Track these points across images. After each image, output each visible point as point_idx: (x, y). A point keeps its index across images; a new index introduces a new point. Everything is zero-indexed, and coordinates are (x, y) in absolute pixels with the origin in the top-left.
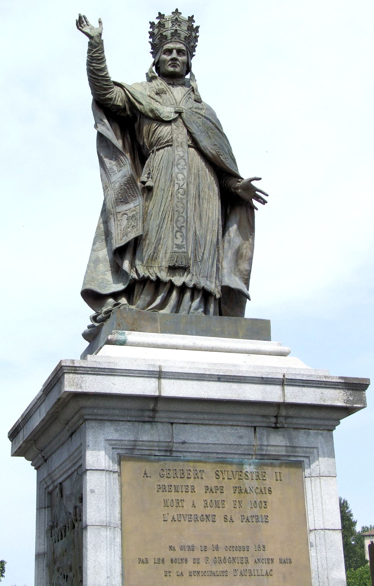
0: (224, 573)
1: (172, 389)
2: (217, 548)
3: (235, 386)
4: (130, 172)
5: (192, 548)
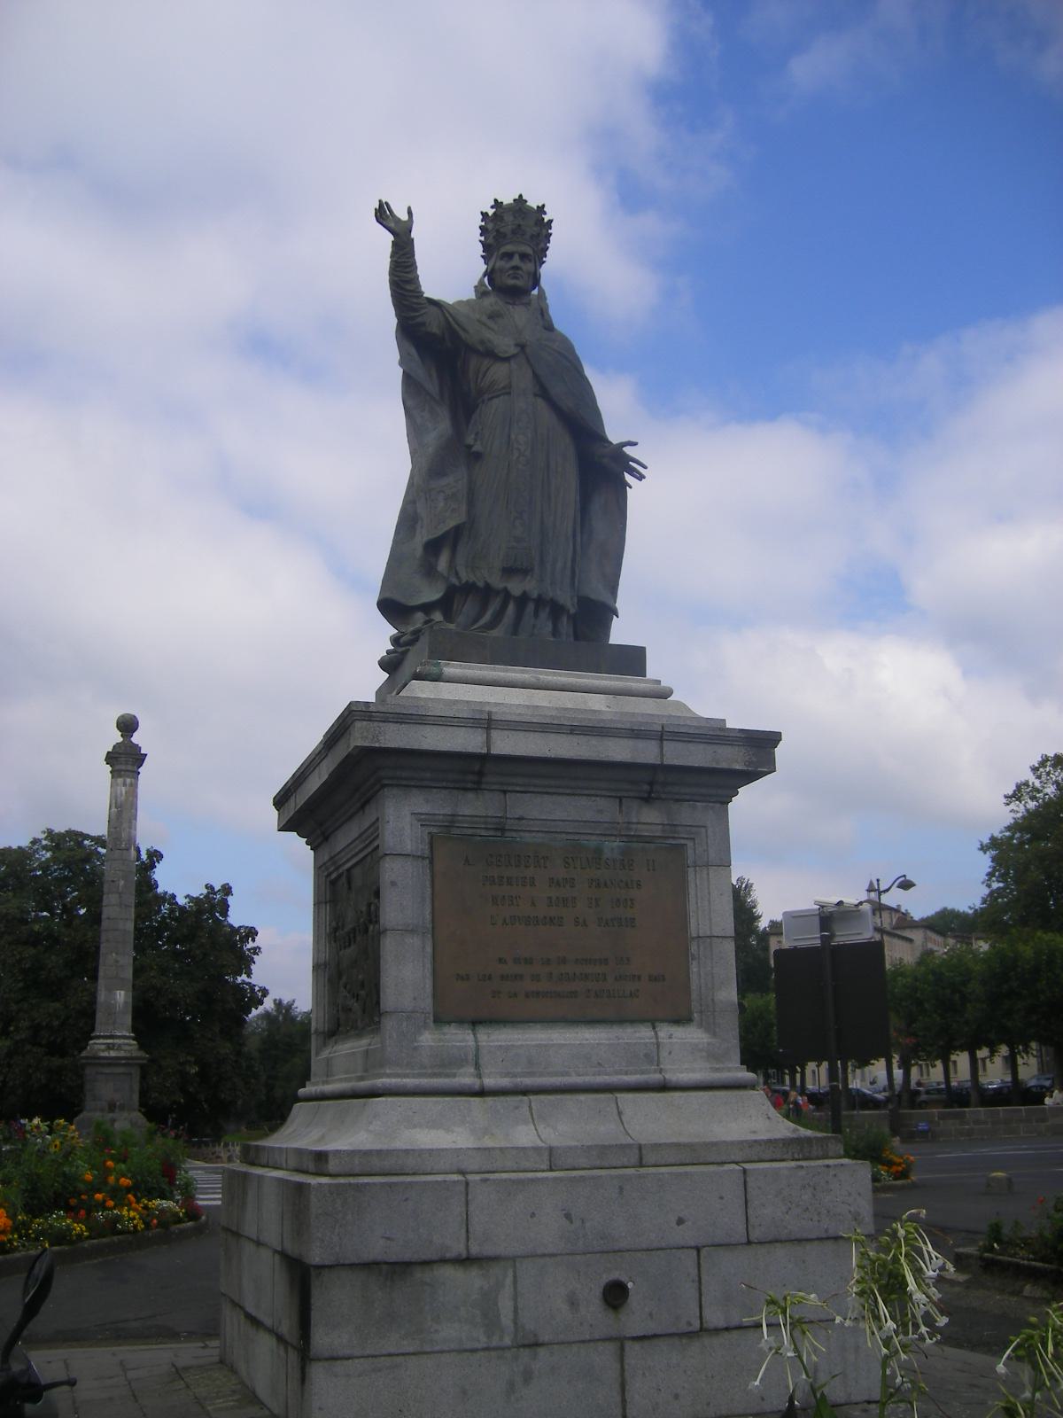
0: (574, 994)
1: (505, 744)
2: (563, 961)
3: (594, 741)
5: (529, 961)
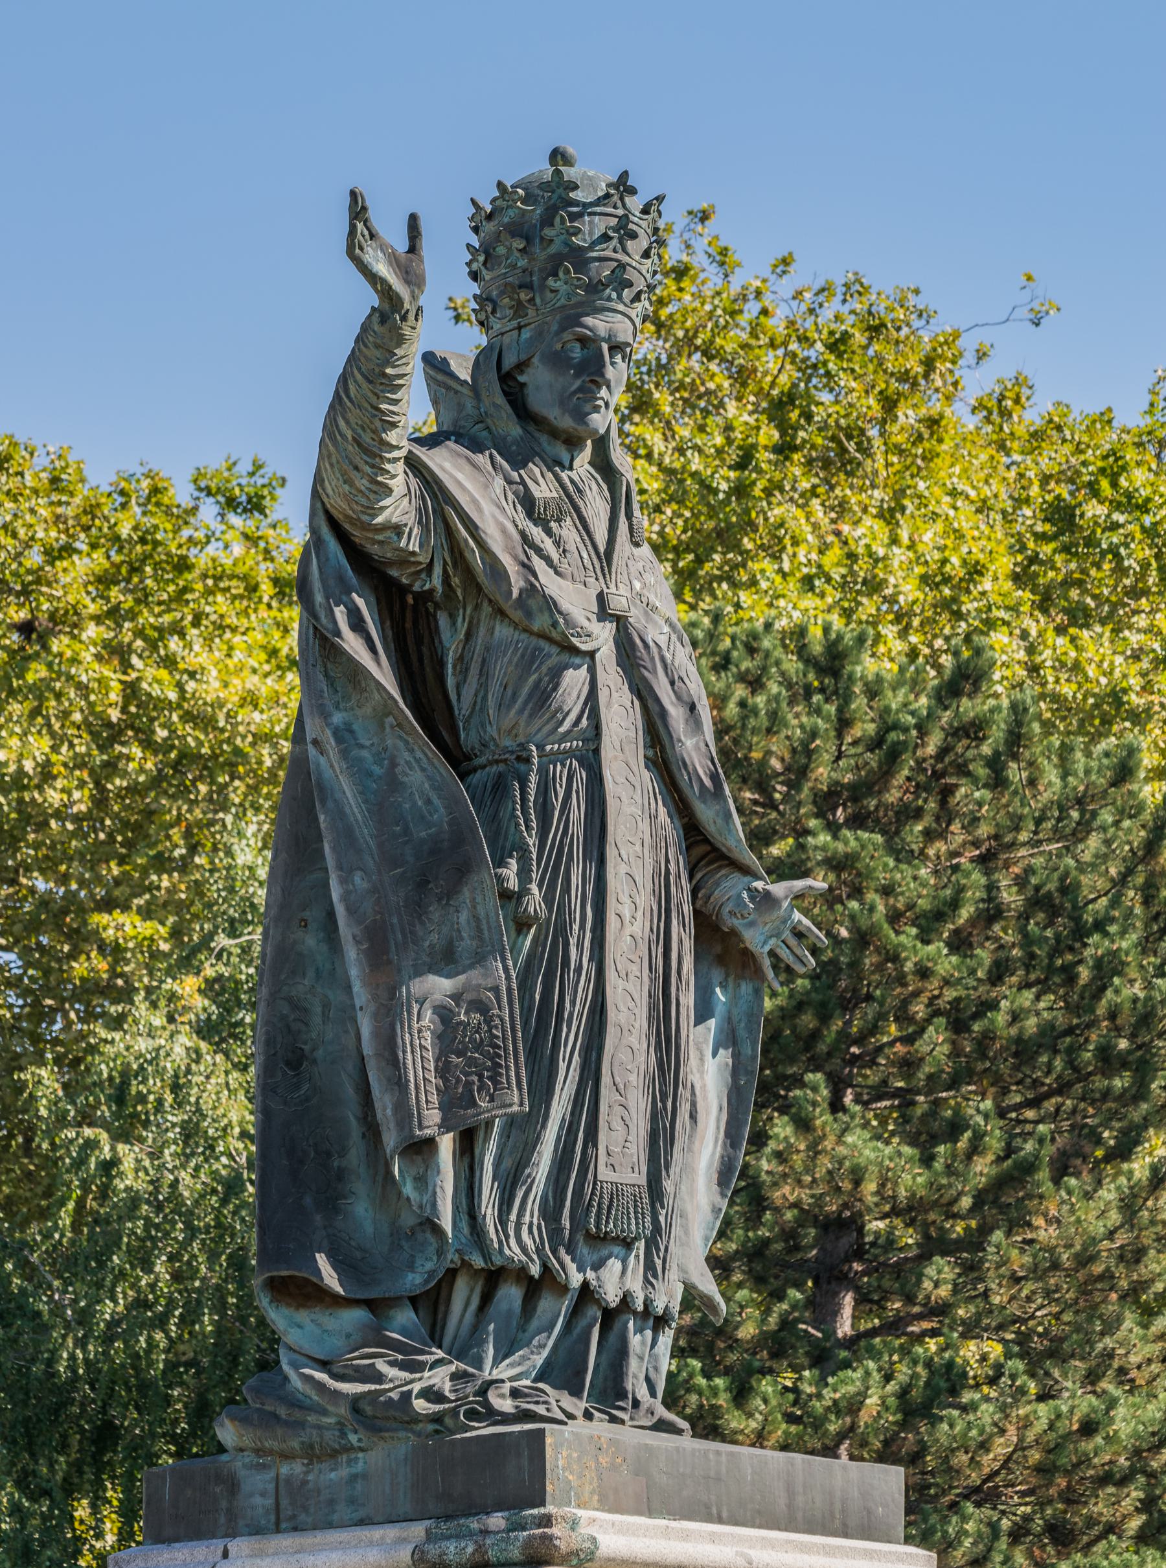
4: (646, 674)
